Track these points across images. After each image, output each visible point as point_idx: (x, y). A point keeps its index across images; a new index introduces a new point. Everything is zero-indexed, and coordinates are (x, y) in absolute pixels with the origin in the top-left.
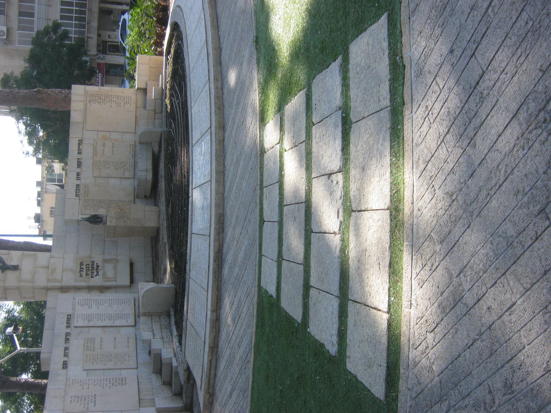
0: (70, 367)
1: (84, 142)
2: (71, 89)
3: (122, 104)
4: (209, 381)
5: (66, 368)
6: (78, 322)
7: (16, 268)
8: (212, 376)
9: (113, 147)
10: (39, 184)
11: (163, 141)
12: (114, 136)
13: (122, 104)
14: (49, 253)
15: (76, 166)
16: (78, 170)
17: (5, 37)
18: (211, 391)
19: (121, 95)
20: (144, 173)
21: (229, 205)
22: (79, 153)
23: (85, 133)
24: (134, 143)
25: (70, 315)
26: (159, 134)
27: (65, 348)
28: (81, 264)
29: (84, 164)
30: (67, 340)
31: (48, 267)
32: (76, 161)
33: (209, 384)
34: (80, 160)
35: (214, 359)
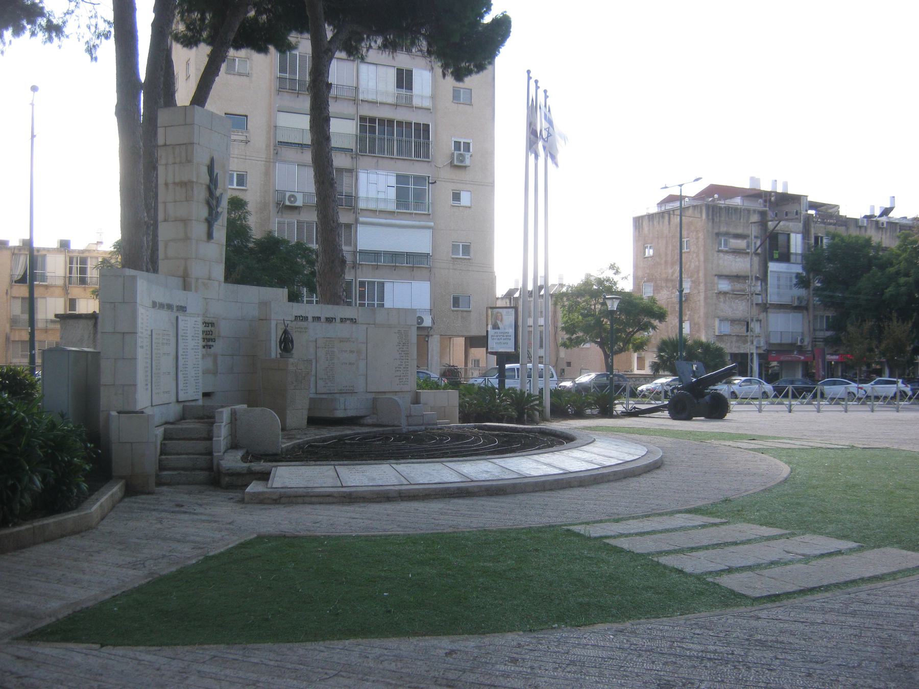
1: (354, 326)
5: (154, 307)
8: (307, 499)
9: (350, 364)
10: (64, 245)
11: (381, 429)
14: (222, 279)
16: (323, 319)
17: (287, 203)
18: (283, 500)
20: (342, 406)
21: (577, 492)
22: (343, 320)
23: (364, 327)
26: (396, 423)
28: (213, 324)
31: (209, 279)
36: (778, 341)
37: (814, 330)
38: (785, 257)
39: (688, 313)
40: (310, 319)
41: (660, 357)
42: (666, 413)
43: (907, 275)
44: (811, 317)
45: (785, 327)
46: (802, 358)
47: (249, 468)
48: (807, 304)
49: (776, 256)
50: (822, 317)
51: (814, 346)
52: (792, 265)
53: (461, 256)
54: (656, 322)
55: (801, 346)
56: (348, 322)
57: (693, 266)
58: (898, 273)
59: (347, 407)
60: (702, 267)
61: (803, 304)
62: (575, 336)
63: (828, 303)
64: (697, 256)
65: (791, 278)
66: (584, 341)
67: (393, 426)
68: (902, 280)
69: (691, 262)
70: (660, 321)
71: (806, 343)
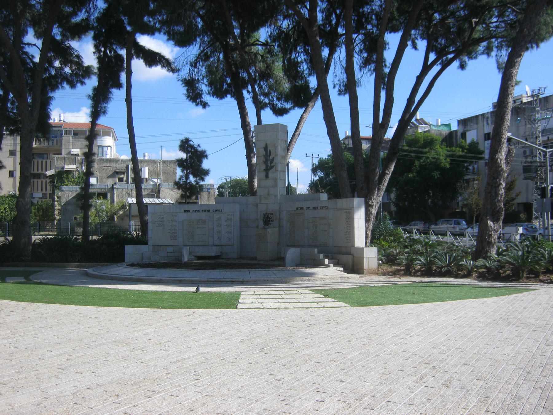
0: (186, 214)
6: (216, 216)
7: (267, 176)
16: (311, 208)
30: (205, 211)
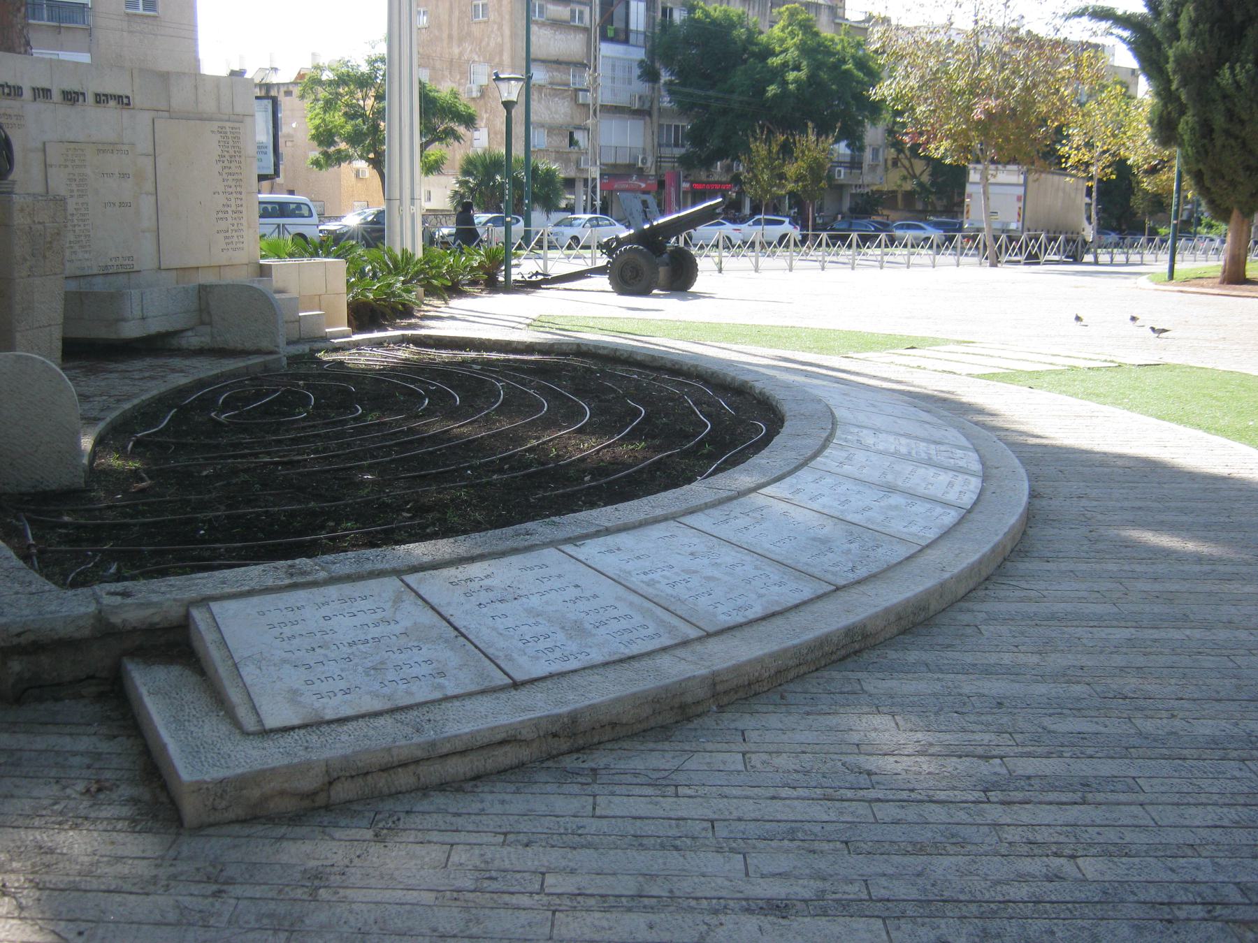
1: (126, 113)
2: (168, 73)
3: (223, 225)
4: (404, 765)
9: (122, 204)
12: (147, 204)
13: (223, 225)
15: (67, 88)
19: (244, 221)
22: (101, 99)
23: (147, 116)
24: (136, 268)
25: (128, 104)
26: (265, 344)
27: (49, 90)
29: (65, 110)
32: (77, 88)
33: (385, 769)
34: (81, 98)
35: (524, 753)
36: (612, 161)
37: (660, 145)
38: (623, 37)
39: (485, 116)
40: (27, 94)
41: (463, 184)
42: (603, 282)
43: (797, 68)
44: (656, 125)
45: (623, 139)
46: (643, 185)
47: (100, 617)
48: (651, 107)
49: (610, 34)
50: (669, 127)
51: (658, 168)
52: (631, 49)
53: (141, 11)
54: (461, 129)
55: (641, 169)
56: (112, 103)
57: (492, 44)
58: (785, 65)
59: (145, 314)
60: (507, 46)
61: (646, 107)
62: (332, 149)
63: (685, 108)
64: (500, 28)
65: (630, 68)
66: (349, 158)
67: (258, 352)
68: (791, 76)
69: (489, 37)
70: (467, 127)
71: (649, 164)
